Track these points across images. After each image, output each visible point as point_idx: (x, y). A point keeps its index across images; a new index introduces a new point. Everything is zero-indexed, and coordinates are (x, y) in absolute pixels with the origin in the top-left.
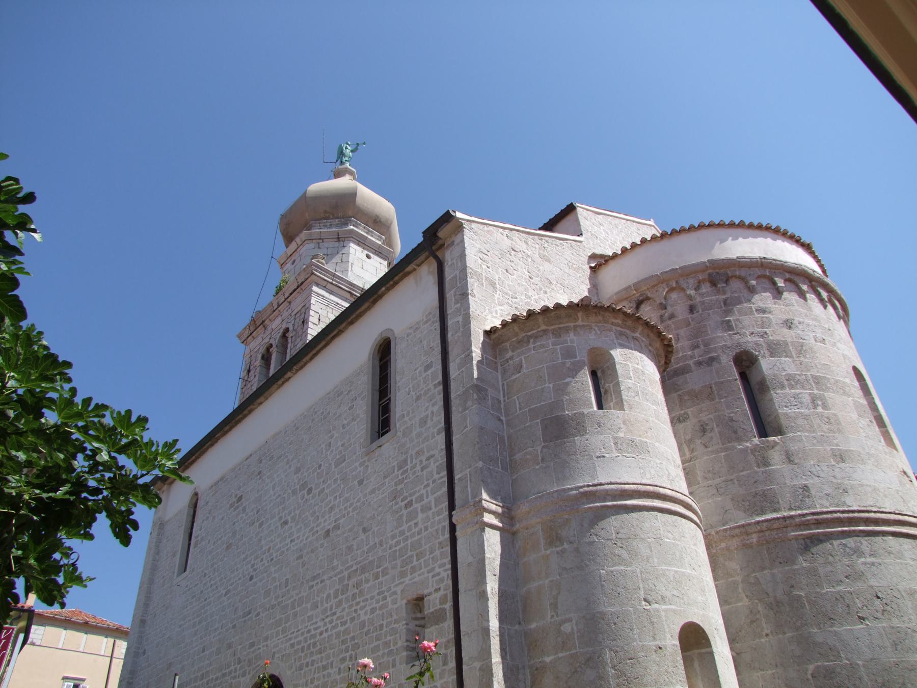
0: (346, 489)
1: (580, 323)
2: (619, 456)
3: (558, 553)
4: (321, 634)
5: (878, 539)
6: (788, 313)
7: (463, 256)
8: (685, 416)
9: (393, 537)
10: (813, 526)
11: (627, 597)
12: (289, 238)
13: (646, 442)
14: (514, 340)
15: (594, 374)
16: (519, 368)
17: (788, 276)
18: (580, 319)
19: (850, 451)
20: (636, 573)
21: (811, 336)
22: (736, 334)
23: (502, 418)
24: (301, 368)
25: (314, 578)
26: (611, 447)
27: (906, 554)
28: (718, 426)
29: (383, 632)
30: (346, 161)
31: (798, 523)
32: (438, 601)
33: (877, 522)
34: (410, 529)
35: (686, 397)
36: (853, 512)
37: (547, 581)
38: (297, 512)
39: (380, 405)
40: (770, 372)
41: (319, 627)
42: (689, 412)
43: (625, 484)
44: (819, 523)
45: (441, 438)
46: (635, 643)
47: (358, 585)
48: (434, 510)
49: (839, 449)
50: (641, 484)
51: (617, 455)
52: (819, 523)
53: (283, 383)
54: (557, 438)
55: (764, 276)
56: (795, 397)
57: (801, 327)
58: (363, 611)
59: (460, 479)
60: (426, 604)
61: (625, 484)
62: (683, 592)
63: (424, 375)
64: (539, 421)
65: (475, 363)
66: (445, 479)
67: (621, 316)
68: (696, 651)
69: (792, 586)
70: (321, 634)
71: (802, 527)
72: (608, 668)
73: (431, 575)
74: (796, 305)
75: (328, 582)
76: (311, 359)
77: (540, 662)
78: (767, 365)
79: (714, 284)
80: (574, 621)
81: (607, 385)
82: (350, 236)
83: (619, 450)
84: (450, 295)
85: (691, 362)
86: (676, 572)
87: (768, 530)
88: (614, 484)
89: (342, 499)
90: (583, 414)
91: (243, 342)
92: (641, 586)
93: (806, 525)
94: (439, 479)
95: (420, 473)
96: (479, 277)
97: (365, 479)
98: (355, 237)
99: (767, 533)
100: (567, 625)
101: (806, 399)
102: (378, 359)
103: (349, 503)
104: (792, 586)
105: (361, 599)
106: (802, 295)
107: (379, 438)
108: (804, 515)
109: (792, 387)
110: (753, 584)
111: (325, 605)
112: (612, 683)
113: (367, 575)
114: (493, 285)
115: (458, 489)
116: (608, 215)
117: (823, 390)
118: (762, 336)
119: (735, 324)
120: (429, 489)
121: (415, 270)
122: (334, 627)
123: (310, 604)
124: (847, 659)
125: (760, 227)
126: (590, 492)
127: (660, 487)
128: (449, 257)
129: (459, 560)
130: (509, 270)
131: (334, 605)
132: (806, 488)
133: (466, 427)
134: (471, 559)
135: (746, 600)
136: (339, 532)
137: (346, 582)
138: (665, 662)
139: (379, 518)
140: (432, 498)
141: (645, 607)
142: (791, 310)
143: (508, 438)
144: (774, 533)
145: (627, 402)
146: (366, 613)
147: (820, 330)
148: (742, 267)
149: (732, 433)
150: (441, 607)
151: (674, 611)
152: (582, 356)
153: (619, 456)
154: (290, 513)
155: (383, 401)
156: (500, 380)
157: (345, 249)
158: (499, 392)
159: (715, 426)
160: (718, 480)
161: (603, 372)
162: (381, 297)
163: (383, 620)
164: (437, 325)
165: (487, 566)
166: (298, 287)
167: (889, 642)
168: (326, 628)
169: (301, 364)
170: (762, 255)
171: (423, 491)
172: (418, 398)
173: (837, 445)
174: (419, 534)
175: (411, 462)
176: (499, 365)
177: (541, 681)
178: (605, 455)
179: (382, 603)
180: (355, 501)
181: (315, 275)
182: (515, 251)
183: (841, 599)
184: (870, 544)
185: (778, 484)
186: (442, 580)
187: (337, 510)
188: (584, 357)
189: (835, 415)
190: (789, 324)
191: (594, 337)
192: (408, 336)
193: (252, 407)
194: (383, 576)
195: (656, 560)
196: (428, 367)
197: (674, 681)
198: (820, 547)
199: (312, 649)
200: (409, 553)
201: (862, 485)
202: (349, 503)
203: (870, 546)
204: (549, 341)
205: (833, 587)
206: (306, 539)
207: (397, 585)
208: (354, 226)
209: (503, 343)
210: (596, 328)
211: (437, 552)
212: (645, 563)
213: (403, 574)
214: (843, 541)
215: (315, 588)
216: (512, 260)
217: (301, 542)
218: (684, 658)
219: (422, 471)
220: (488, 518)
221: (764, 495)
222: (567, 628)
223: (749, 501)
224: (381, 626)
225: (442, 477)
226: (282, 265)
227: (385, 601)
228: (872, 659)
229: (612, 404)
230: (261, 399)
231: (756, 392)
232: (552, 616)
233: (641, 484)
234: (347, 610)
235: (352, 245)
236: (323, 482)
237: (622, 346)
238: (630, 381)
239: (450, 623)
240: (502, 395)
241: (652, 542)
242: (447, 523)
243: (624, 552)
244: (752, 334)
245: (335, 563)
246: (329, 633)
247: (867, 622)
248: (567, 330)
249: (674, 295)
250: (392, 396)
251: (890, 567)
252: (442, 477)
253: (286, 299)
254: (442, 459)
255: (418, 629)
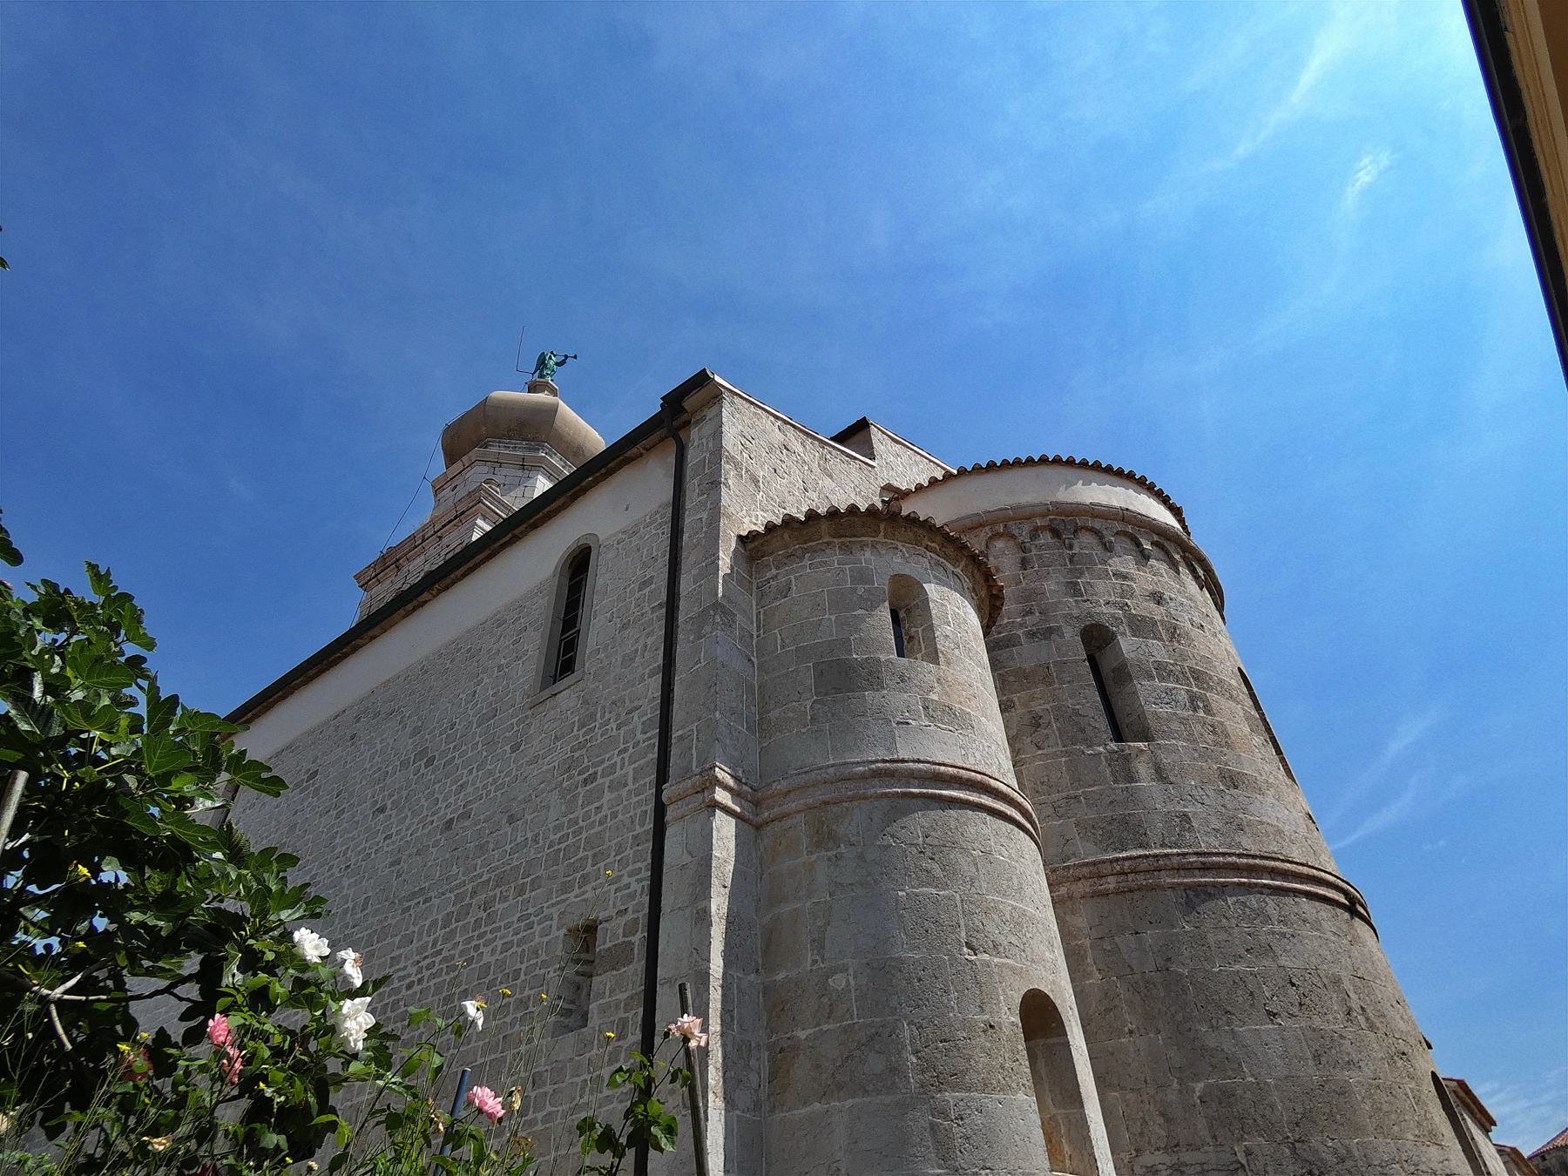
0: (490, 758)
1: (881, 538)
2: (930, 726)
3: (829, 859)
4: (409, 987)
5: (1289, 900)
6: (1156, 584)
7: (718, 434)
8: (1009, 703)
9: (558, 828)
10: (1196, 872)
11: (939, 938)
12: (452, 456)
13: (969, 713)
14: (780, 552)
15: (894, 614)
16: (786, 590)
17: (1156, 538)
18: (882, 534)
19: (1243, 774)
20: (954, 900)
21: (1186, 618)
22: (1085, 601)
23: (752, 658)
24: (447, 588)
25: (413, 895)
26: (919, 711)
27: (1325, 925)
28: (1057, 720)
29: (518, 982)
30: (548, 374)
31: (1176, 866)
32: (621, 931)
33: (1286, 875)
34: (587, 816)
35: (1011, 679)
36: (1254, 857)
37: (808, 904)
38: (404, 793)
39: (561, 641)
40: (1132, 655)
41: (410, 975)
42: (1015, 699)
43: (939, 764)
44: (1206, 868)
45: (655, 684)
46: (951, 1015)
47: (486, 906)
48: (631, 786)
49: (1230, 770)
50: (963, 768)
51: (927, 723)
52: (1206, 868)
53: (414, 609)
54: (838, 690)
55: (1125, 533)
56: (1168, 692)
57: (1172, 604)
58: (490, 948)
59: (681, 738)
60: (599, 934)
61: (939, 764)
62: (1024, 940)
63: (637, 595)
64: (811, 664)
65: (721, 574)
66: (656, 741)
67: (939, 538)
68: (1042, 1042)
69: (1169, 959)
70: (409, 987)
71: (1182, 872)
72: (905, 1054)
73: (613, 888)
74: (1165, 576)
75: (436, 901)
76: (464, 575)
77: (789, 1038)
78: (1127, 644)
79: (1056, 533)
80: (851, 971)
81: (914, 629)
82: (540, 465)
83: (931, 717)
84: (692, 485)
85: (1020, 632)
86: (1014, 908)
87: (1132, 872)
88: (923, 762)
89: (480, 773)
90: (879, 660)
91: (361, 587)
92: (962, 922)
93: (1188, 869)
94: (644, 742)
95: (614, 733)
96: (737, 465)
97: (524, 743)
98: (546, 467)
99: (1130, 877)
100: (838, 976)
101: (1183, 697)
102: (568, 577)
103: (491, 780)
104: (1169, 959)
105: (489, 928)
106: (1174, 566)
107: (554, 683)
108: (1184, 855)
109: (1162, 679)
110: (1109, 951)
111: (425, 939)
112: (912, 1081)
113: (504, 888)
114: (756, 481)
115: (675, 751)
116: (908, 448)
117: (1204, 689)
118: (1121, 608)
119: (1084, 588)
120: (626, 755)
121: (641, 455)
122: (434, 976)
123: (399, 937)
124: (1252, 1075)
125: (1120, 473)
126: (887, 770)
127: (990, 777)
128: (696, 437)
129: (667, 859)
130: (778, 471)
131: (441, 939)
132: (1185, 817)
133: (699, 661)
134: (687, 859)
135: (1098, 976)
136: (467, 823)
137: (467, 901)
138: (999, 1050)
139: (539, 800)
140: (630, 770)
141: (967, 957)
142: (1159, 581)
143: (760, 687)
144: (1140, 877)
145: (943, 654)
146: (493, 951)
147: (1197, 614)
148: (1096, 517)
149: (1075, 731)
150: (626, 939)
151: (1013, 969)
152: (882, 583)
153: (930, 726)
154: (391, 796)
155: (567, 635)
156: (754, 607)
157: (531, 481)
158: (752, 623)
159: (1053, 720)
160: (1055, 796)
161: (908, 611)
162: (584, 491)
163: (521, 963)
164: (667, 528)
165: (713, 869)
166: (456, 518)
167: (1311, 1052)
168: (420, 976)
169: (448, 581)
170: (1124, 506)
171: (618, 759)
172: (625, 627)
173: (1226, 764)
174: (601, 823)
175: (603, 716)
176: (754, 586)
177: (788, 1071)
178: (910, 721)
179: (525, 934)
180: (503, 775)
181: (484, 504)
182: (788, 450)
183: (1241, 983)
184: (1278, 906)
185: (1145, 808)
186: (632, 896)
187: (470, 789)
188: (884, 585)
189: (1222, 723)
190: (1158, 598)
191: (899, 561)
192: (618, 544)
193: (359, 641)
194: (531, 891)
195: (984, 885)
196: (645, 584)
197: (1014, 1085)
198: (1211, 904)
199: (389, 1013)
200: (581, 854)
201: (1262, 823)
202: (491, 780)
203: (1278, 908)
204: (835, 558)
205: (1229, 963)
206: (411, 835)
207: (553, 905)
208: (546, 453)
209: (763, 556)
210: (904, 550)
211: (629, 852)
212: (969, 887)
213: (566, 887)
214: (1242, 899)
215: (412, 912)
216: (783, 459)
217: (401, 840)
218: (1028, 1049)
219: (618, 728)
220: (722, 796)
221: (1125, 822)
222: (838, 982)
223: (1102, 829)
224: (517, 973)
225: (650, 738)
226: (436, 493)
227: (529, 931)
228: (1287, 1077)
229: (919, 656)
230: (377, 630)
231: (1109, 683)
232: (815, 962)
233: (963, 768)
234: (461, 947)
235: (540, 477)
236: (454, 748)
237: (940, 582)
238: (948, 628)
239: (638, 966)
240: (755, 630)
241: (979, 856)
242: (650, 807)
243: (935, 866)
244: (1108, 603)
245: (455, 870)
246: (425, 985)
247: (1279, 1020)
248: (863, 546)
249: (1000, 544)
250: (583, 628)
251: (1307, 941)
252: (650, 738)
253: (435, 532)
254: (652, 711)
255: (579, 979)
